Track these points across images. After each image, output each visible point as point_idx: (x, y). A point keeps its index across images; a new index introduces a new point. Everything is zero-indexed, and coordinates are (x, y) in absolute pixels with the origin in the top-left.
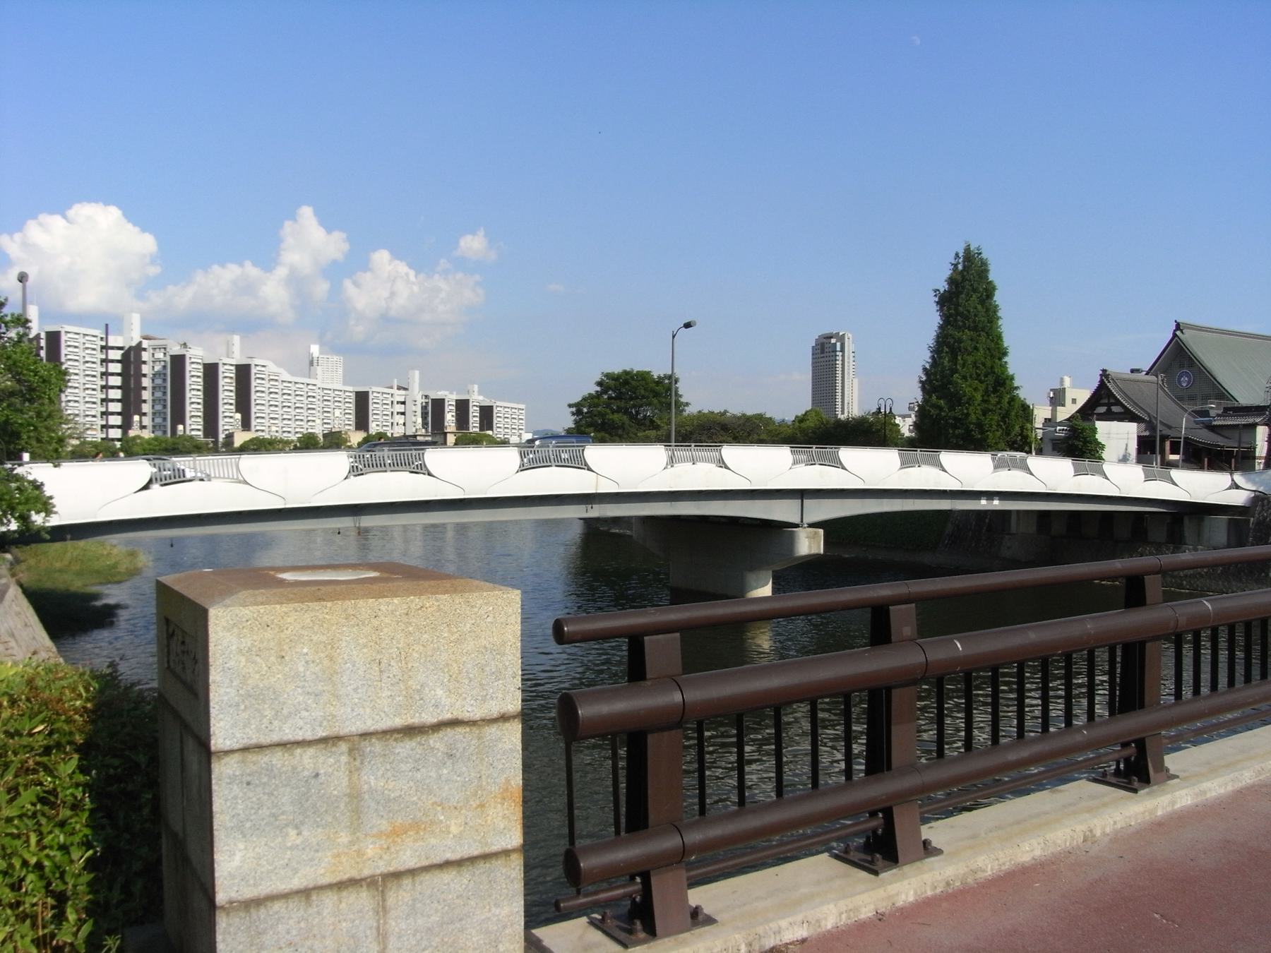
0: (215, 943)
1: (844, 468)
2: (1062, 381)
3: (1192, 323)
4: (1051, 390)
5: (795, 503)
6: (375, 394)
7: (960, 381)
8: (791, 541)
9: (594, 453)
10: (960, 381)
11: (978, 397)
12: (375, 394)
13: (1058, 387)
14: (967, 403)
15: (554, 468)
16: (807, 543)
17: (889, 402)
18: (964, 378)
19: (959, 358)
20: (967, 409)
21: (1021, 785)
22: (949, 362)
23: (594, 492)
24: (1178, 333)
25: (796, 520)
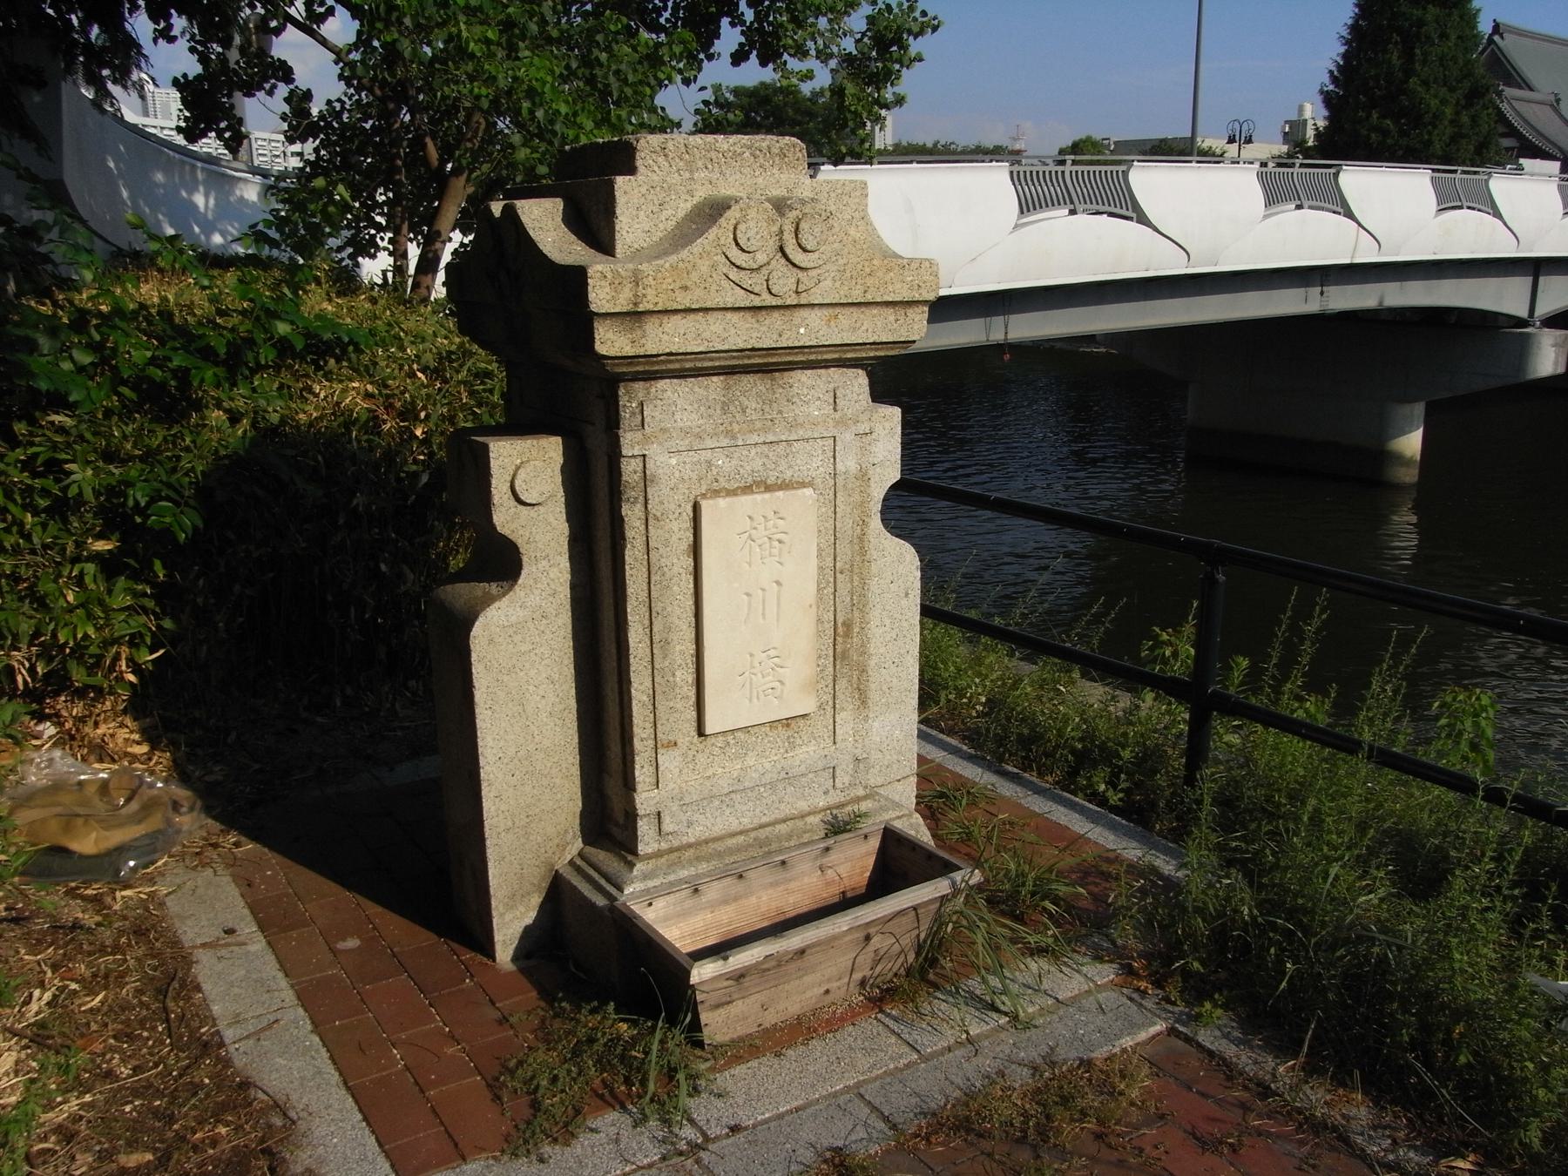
0: (470, 664)
1: (1143, 219)
2: (1301, 109)
3: (1517, 25)
4: (1286, 122)
5: (1521, 285)
6: (260, 142)
7: (1419, 89)
8: (1523, 348)
9: (1357, 180)
10: (1419, 89)
11: (1448, 111)
12: (260, 142)
13: (1295, 118)
14: (1430, 123)
15: (1465, 211)
16: (1553, 355)
17: (1245, 127)
18: (1425, 83)
19: (1418, 51)
20: (1430, 133)
21: (930, 478)
22: (1399, 58)
23: (1347, 261)
24: (1496, 38)
25: (1523, 312)
